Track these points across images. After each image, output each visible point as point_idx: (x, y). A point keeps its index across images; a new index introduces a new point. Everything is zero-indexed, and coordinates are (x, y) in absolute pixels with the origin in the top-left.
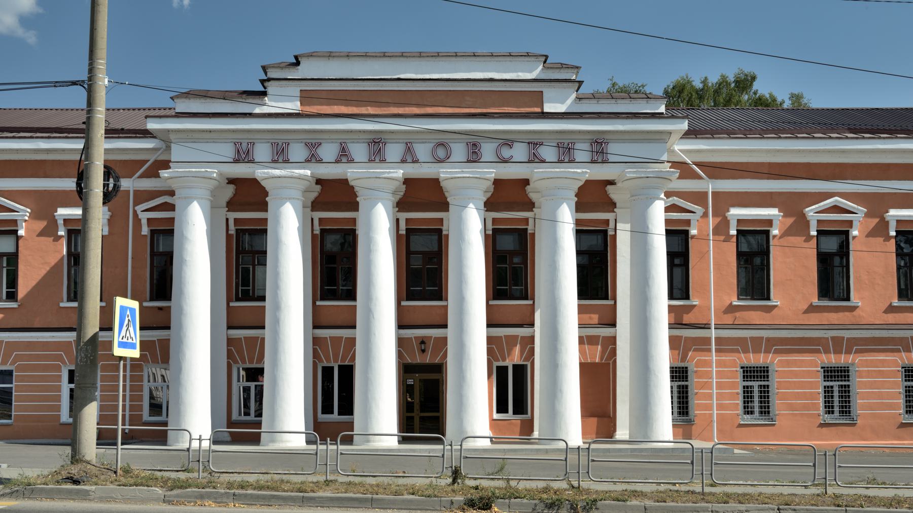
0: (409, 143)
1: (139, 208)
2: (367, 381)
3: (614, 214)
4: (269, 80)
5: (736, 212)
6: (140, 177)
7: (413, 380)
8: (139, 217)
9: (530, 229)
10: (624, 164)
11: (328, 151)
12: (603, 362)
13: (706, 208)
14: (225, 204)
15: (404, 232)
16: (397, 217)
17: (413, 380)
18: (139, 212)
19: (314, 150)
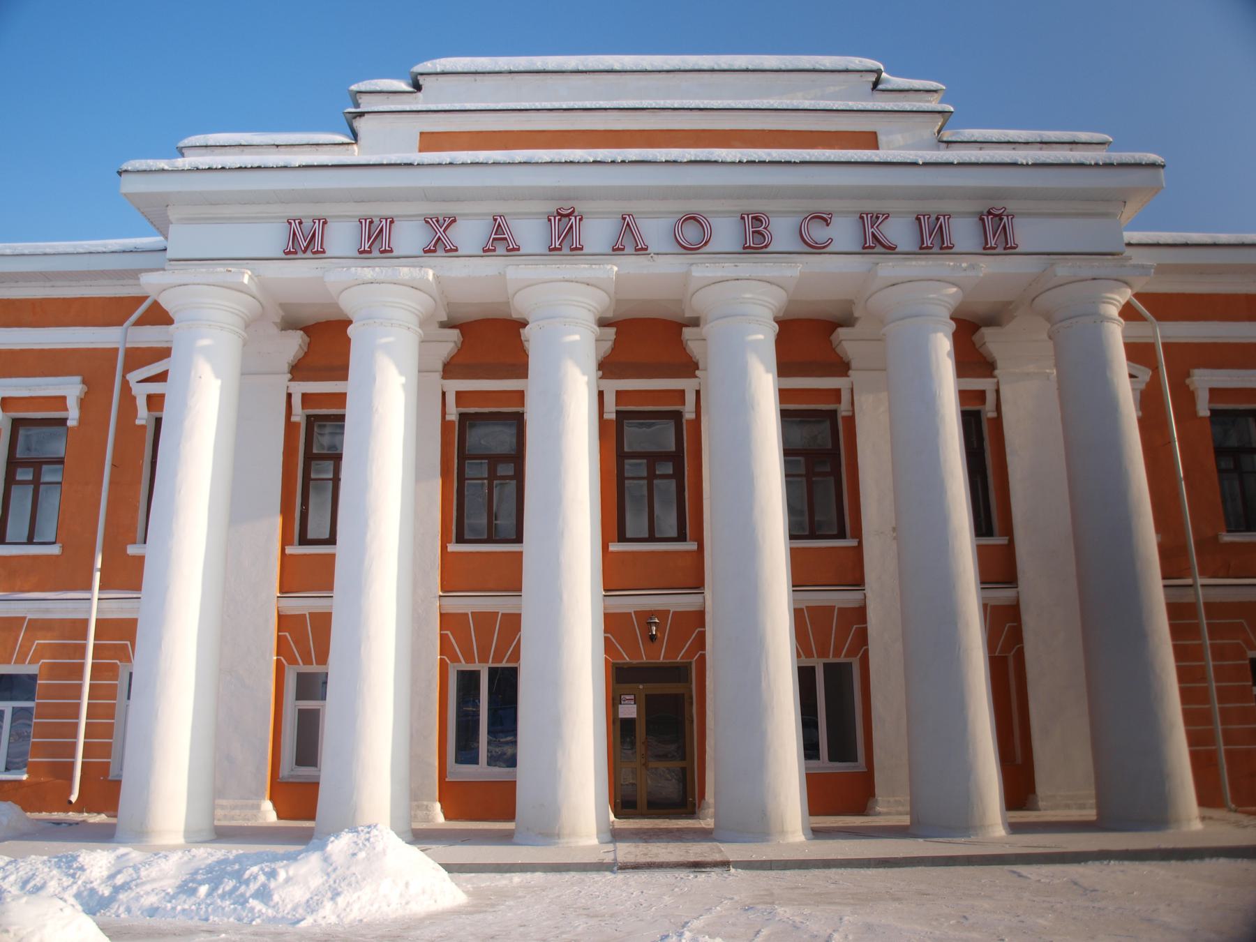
0: (629, 215)
1: (133, 377)
2: (415, 737)
3: (995, 380)
4: (362, 114)
5: (1204, 380)
7: (632, 697)
8: (133, 393)
9: (843, 409)
10: (1046, 256)
11: (469, 234)
12: (996, 654)
13: (1155, 369)
14: (286, 368)
15: (613, 416)
16: (601, 389)
17: (632, 697)
18: (133, 384)
19: (441, 230)
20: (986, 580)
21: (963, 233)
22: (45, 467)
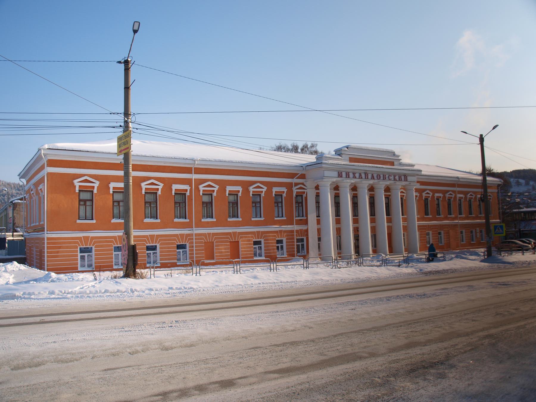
6: (296, 178)
20: (371, 222)
21: (351, 175)
22: (257, 203)
